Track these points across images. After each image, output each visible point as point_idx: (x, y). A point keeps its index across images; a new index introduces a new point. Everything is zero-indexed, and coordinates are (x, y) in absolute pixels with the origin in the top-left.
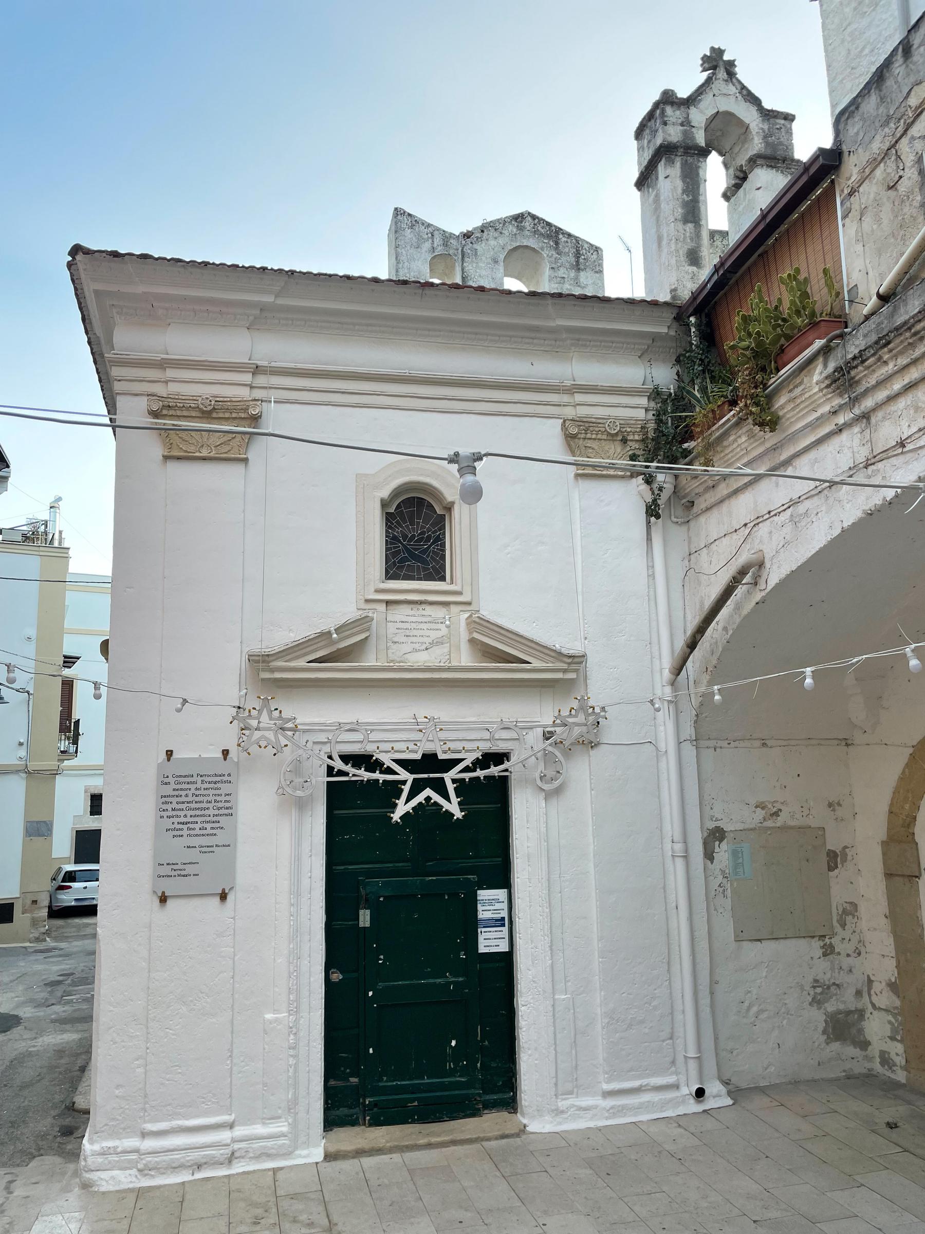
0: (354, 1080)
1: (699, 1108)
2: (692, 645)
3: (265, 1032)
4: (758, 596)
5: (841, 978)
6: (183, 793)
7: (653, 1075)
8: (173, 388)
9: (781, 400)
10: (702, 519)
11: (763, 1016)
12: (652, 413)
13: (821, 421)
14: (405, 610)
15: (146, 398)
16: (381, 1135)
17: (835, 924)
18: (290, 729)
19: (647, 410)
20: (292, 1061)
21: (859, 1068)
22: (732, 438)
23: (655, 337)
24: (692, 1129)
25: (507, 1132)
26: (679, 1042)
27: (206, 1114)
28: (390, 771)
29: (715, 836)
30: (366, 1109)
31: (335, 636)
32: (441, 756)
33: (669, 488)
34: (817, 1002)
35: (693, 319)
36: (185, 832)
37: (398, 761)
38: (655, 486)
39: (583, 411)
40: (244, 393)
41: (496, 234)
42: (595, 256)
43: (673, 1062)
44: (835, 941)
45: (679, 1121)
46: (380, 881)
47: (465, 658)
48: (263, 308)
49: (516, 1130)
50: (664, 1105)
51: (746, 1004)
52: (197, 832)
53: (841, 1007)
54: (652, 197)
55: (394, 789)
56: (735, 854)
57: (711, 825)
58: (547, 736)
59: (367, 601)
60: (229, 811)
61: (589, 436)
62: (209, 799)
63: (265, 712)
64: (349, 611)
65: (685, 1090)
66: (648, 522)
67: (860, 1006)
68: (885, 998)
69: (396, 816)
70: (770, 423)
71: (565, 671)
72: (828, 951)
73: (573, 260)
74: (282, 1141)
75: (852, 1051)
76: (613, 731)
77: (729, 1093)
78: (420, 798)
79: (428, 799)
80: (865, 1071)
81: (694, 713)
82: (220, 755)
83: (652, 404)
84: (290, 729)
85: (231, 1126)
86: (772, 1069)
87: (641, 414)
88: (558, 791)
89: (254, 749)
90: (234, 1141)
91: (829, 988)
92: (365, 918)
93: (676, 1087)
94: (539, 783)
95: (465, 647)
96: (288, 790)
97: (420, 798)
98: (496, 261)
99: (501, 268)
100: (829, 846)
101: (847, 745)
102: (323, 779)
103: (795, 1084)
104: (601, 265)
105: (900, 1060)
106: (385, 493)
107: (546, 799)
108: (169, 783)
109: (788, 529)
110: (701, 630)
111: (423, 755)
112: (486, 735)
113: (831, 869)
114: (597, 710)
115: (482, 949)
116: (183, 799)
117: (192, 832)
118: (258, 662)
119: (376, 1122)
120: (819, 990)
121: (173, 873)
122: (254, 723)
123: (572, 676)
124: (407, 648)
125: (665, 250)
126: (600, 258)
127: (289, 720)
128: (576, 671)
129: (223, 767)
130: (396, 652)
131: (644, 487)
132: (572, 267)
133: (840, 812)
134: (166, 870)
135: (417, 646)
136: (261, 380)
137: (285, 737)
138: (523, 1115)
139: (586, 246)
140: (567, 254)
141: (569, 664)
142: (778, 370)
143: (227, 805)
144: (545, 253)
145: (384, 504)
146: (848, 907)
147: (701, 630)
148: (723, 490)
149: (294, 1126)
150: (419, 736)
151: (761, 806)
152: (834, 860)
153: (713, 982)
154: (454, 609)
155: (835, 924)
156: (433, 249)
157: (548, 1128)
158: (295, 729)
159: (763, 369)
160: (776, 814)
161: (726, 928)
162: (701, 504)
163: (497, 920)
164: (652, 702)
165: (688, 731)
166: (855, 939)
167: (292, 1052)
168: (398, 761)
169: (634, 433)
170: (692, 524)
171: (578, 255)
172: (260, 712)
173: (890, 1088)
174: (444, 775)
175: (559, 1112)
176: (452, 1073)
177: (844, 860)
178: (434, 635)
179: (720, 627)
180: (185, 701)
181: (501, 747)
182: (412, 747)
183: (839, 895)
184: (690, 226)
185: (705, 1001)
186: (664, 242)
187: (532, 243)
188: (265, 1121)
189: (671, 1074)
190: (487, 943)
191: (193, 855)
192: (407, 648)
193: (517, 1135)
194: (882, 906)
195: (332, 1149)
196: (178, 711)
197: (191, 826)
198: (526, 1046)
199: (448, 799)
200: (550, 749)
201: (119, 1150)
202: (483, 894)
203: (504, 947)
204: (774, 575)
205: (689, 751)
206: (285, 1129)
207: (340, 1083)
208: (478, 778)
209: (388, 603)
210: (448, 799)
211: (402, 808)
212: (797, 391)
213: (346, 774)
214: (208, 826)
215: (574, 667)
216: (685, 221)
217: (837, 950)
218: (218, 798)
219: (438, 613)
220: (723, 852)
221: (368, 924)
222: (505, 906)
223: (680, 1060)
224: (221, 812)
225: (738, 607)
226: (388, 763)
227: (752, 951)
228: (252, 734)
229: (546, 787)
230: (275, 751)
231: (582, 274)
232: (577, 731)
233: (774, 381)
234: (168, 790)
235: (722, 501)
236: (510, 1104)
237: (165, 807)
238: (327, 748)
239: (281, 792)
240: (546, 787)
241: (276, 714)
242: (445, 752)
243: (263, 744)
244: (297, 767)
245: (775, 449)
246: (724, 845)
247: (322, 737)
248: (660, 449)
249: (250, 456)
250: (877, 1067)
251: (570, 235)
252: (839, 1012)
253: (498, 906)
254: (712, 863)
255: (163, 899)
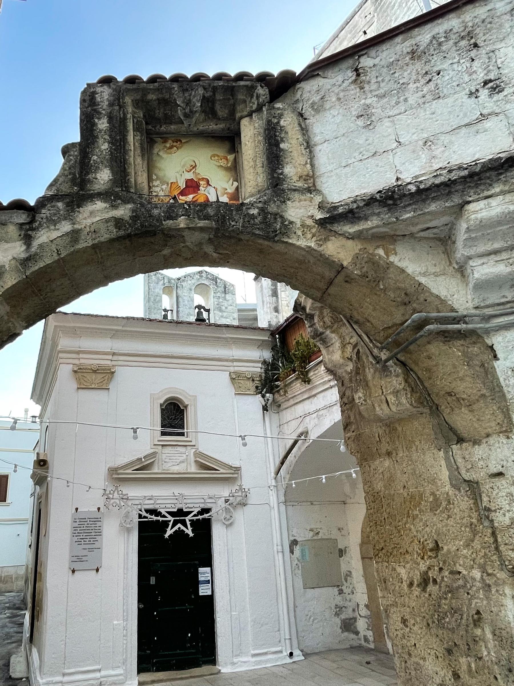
0: (148, 652)
1: (291, 661)
2: (282, 463)
3: (114, 629)
4: (307, 445)
5: (347, 604)
6: (82, 526)
7: (273, 647)
8: (82, 361)
9: (311, 374)
10: (284, 412)
11: (316, 621)
12: (263, 369)
13: (324, 383)
14: (170, 448)
15: (72, 365)
16: (161, 675)
17: (343, 580)
18: (125, 499)
19: (261, 368)
20: (125, 642)
21: (355, 644)
22: (294, 384)
23: (263, 341)
24: (289, 668)
25: (213, 672)
26: (282, 632)
27: (90, 665)
28: (164, 516)
29: (294, 543)
30: (154, 665)
31: (143, 460)
32: (185, 510)
33: (271, 399)
34: (337, 614)
35: (277, 336)
36: (83, 543)
37: (167, 512)
38: (266, 399)
39: (237, 369)
40: (109, 362)
41: (191, 279)
42: (232, 288)
43: (280, 641)
44: (344, 588)
45: (283, 666)
46: (159, 565)
47: (193, 468)
48: (117, 331)
49: (216, 672)
50: (277, 660)
51: (308, 617)
52: (87, 542)
53: (347, 616)
54: (260, 285)
55: (166, 524)
56: (302, 551)
57: (292, 538)
58: (227, 501)
59: (155, 445)
60: (99, 533)
61: (240, 378)
62: (92, 528)
63: (116, 492)
64: (149, 451)
65: (285, 654)
66: (263, 412)
67: (355, 616)
68: (364, 611)
69: (166, 536)
70: (307, 381)
71: (233, 474)
72: (341, 592)
73: (223, 290)
74: (121, 677)
75: (353, 636)
76: (253, 499)
77: (303, 655)
78: (176, 528)
79: (179, 528)
80: (358, 645)
81: (284, 491)
82: (97, 510)
83: (263, 367)
84: (125, 499)
85: (99, 670)
86: (320, 645)
87: (259, 370)
88: (231, 524)
89: (110, 507)
90: (102, 677)
91: (342, 608)
92: (153, 580)
93: (281, 652)
94: (224, 521)
95: (193, 464)
96: (124, 524)
97: (176, 528)
98: (191, 290)
99: (193, 292)
100: (340, 547)
101: (345, 504)
102: (137, 520)
103: (330, 651)
104: (234, 292)
105: (371, 639)
106: (162, 401)
107: (226, 528)
108: (76, 522)
109: (316, 420)
110: (286, 457)
111: (178, 510)
112: (203, 501)
113: (341, 557)
114: (246, 490)
115: (201, 594)
116: (82, 528)
117: (85, 543)
118: (113, 470)
119: (158, 670)
120: (338, 609)
121: (78, 560)
122: (111, 496)
123: (236, 476)
124: (169, 465)
125: (265, 306)
126: (234, 289)
127: (125, 495)
128: (238, 473)
129: (98, 515)
130: (166, 466)
131: (261, 399)
132: (223, 292)
133: (343, 532)
134: (75, 559)
135: (174, 463)
136: (115, 358)
137: (123, 502)
138: (219, 666)
139: (228, 284)
140: (221, 287)
141: (235, 471)
142: (310, 363)
143: (99, 531)
144: (211, 287)
145: (161, 405)
146: (348, 573)
147: (286, 457)
148: (292, 402)
149: (126, 670)
150: (176, 501)
151: (311, 530)
152: (341, 553)
153: (295, 606)
154: (189, 448)
155: (343, 580)
156: (164, 284)
157: (230, 671)
158: (127, 499)
159: (304, 362)
160: (318, 533)
161: (299, 583)
162: (283, 406)
163: (206, 581)
164: (269, 487)
165: (282, 499)
166: (351, 587)
167: (125, 638)
168: (167, 512)
169: (257, 377)
170: (280, 413)
171: (225, 287)
172: (114, 492)
173: (368, 651)
174: (186, 518)
175: (233, 664)
176: (189, 648)
177: (345, 553)
178: (181, 459)
179: (293, 455)
180: (90, 487)
181: (208, 506)
182: (173, 506)
183: (344, 568)
184: (275, 298)
185: (292, 614)
186: (265, 303)
187: (206, 282)
188: (113, 668)
189: (280, 646)
190: (203, 591)
191: (85, 552)
192: (169, 465)
193: (217, 674)
194: (361, 572)
195: (142, 680)
196: (87, 491)
197: (85, 540)
198: (220, 635)
199: (187, 528)
200: (228, 506)
201: (54, 682)
202: (201, 570)
203: (209, 593)
204: (313, 436)
205: (283, 507)
206: (122, 672)
207: (143, 653)
208: (199, 519)
209: (163, 445)
210: (187, 528)
211: (169, 532)
212: (317, 371)
213: (147, 518)
214: (92, 540)
215: (236, 472)
216: (273, 296)
217: (344, 592)
218: (96, 528)
219: (182, 449)
220: (297, 550)
221: (154, 583)
222: (210, 575)
223: (283, 640)
224: (97, 534)
225: (299, 448)
226: (164, 513)
227: (310, 593)
228: (110, 501)
229: (226, 523)
230: (119, 508)
231: (227, 295)
232: (239, 499)
233: (308, 367)
234: (76, 525)
235: (291, 406)
236: (213, 662)
237: (75, 532)
238: (139, 507)
239: (121, 525)
240: (226, 523)
241: (120, 492)
242: (186, 508)
243: (114, 505)
244: (127, 515)
245: (310, 389)
246: (298, 547)
247: (137, 502)
248: (267, 384)
249: (110, 387)
250: (363, 642)
251: (221, 280)
252: (347, 619)
253: (207, 575)
254: (293, 554)
255: (73, 571)
